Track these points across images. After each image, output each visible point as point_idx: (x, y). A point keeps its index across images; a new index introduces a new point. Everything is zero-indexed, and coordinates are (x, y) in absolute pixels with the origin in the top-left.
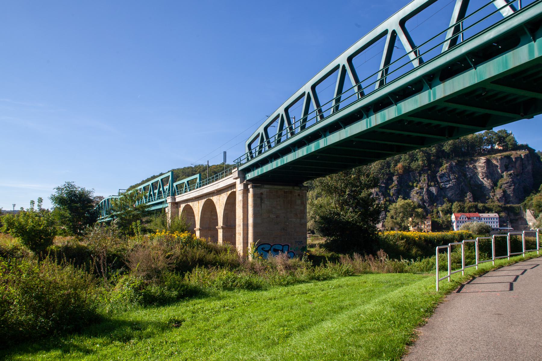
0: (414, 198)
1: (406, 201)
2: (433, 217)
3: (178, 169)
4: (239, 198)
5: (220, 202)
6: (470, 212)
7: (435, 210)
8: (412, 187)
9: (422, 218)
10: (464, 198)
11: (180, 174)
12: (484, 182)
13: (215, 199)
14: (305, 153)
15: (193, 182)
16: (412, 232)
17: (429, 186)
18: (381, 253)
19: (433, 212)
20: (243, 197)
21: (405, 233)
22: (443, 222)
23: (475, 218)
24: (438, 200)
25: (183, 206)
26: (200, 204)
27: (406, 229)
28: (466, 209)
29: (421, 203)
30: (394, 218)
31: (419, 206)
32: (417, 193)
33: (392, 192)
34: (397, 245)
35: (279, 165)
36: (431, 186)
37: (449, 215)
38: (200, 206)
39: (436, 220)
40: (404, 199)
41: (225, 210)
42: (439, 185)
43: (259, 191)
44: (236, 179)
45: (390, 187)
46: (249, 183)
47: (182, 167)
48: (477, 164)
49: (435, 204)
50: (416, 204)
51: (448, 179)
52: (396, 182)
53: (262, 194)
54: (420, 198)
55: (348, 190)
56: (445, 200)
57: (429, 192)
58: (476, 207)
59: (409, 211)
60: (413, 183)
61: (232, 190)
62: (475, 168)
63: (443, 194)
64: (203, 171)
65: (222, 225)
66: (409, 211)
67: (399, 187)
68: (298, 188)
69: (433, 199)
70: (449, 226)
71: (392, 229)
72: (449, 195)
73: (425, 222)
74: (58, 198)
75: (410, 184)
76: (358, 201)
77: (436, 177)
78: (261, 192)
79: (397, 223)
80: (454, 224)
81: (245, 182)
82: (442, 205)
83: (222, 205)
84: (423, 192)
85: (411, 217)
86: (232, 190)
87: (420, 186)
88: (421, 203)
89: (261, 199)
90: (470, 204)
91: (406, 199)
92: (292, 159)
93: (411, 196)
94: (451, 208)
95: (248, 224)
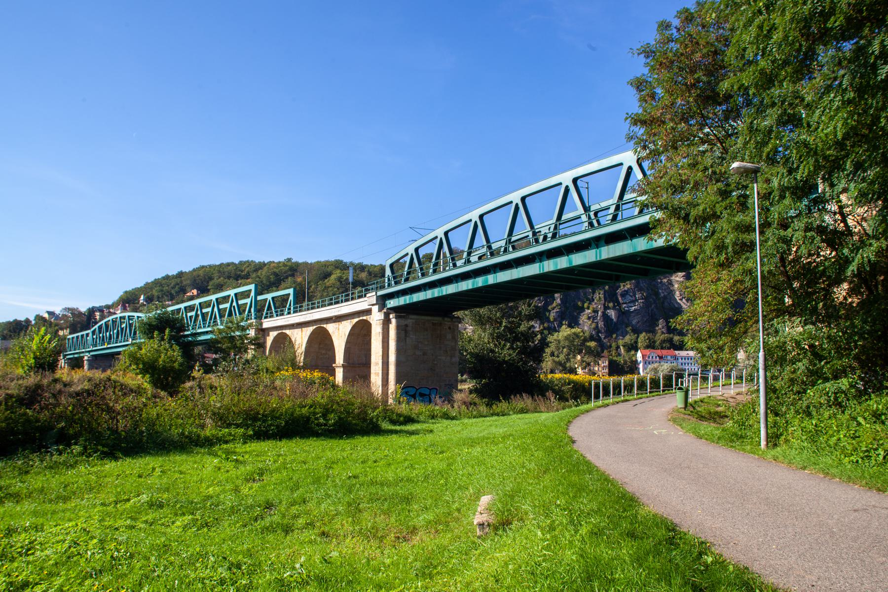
0: (584, 326)
1: (573, 330)
2: (611, 355)
3: (210, 266)
4: (376, 331)
5: (340, 334)
6: (662, 348)
7: (614, 345)
8: (582, 309)
9: (595, 356)
10: (655, 327)
11: (215, 275)
12: (682, 304)
13: (330, 327)
14: (470, 287)
15: (285, 298)
16: (581, 375)
17: (606, 308)
18: (550, 394)
19: (611, 346)
20: (383, 329)
21: (573, 377)
22: (625, 362)
23: (669, 358)
24: (617, 330)
25: (273, 334)
26: (304, 333)
27: (573, 371)
28: (658, 343)
29: (593, 333)
30: (556, 354)
31: (592, 338)
32: (589, 318)
33: (552, 315)
34: (563, 391)
35: (436, 295)
36: (608, 308)
37: (633, 352)
38: (304, 335)
39: (615, 358)
40: (570, 326)
41: (348, 342)
42: (620, 307)
43: (403, 322)
44: (373, 305)
45: (550, 308)
46: (390, 311)
47: (218, 263)
48: (673, 278)
49: (614, 336)
50: (587, 334)
51: (633, 298)
52: (559, 301)
53: (406, 326)
54: (594, 325)
55: (504, 321)
56: (628, 329)
57: (606, 317)
58: (670, 341)
59: (577, 346)
60: (583, 303)
61: (361, 318)
62: (671, 283)
63: (626, 321)
64: (255, 271)
65: (342, 362)
66: (577, 346)
67: (563, 309)
68: (449, 320)
69: (612, 328)
70: (633, 368)
71: (552, 372)
72: (634, 322)
73: (600, 362)
74: (146, 324)
75: (579, 304)
76: (517, 335)
77: (616, 294)
78: (406, 323)
79: (560, 363)
80: (641, 366)
81: (385, 310)
82: (624, 337)
83: (343, 336)
84: (597, 317)
85: (579, 353)
86: (361, 318)
87: (593, 308)
88: (593, 333)
89: (406, 332)
90: (662, 337)
91: (573, 327)
92: (454, 291)
93: (581, 322)
94: (636, 342)
95: (388, 362)
